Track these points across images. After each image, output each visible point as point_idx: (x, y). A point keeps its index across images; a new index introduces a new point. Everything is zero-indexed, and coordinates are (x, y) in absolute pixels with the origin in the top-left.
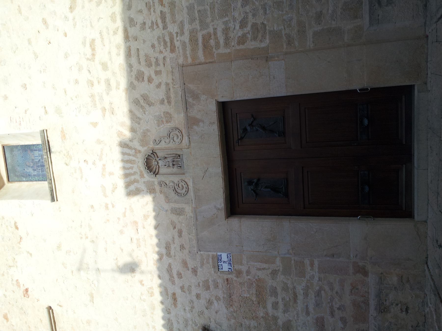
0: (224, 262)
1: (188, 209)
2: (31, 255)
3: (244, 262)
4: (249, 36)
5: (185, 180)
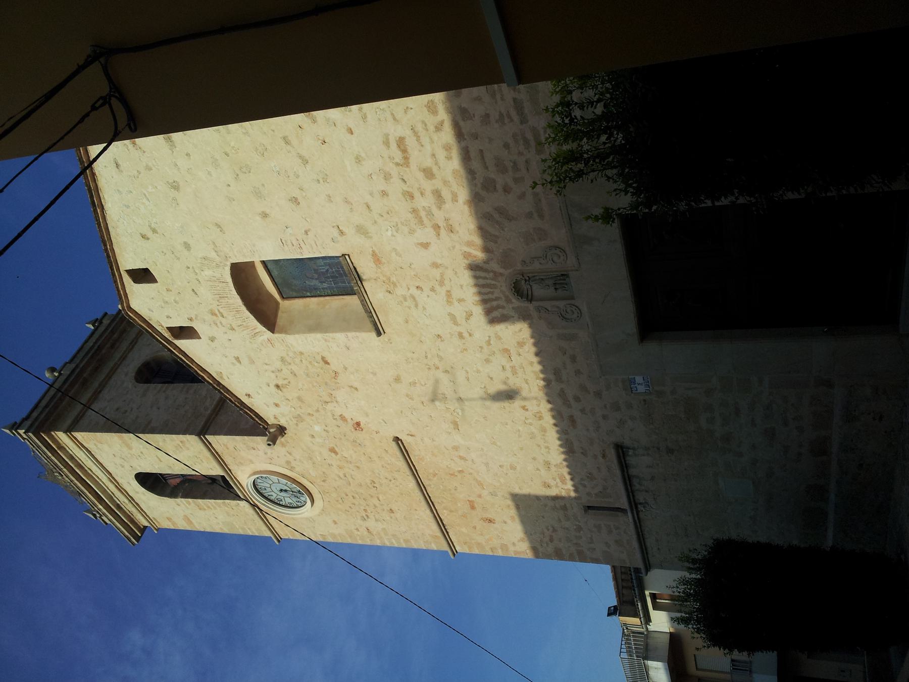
2: (356, 389)
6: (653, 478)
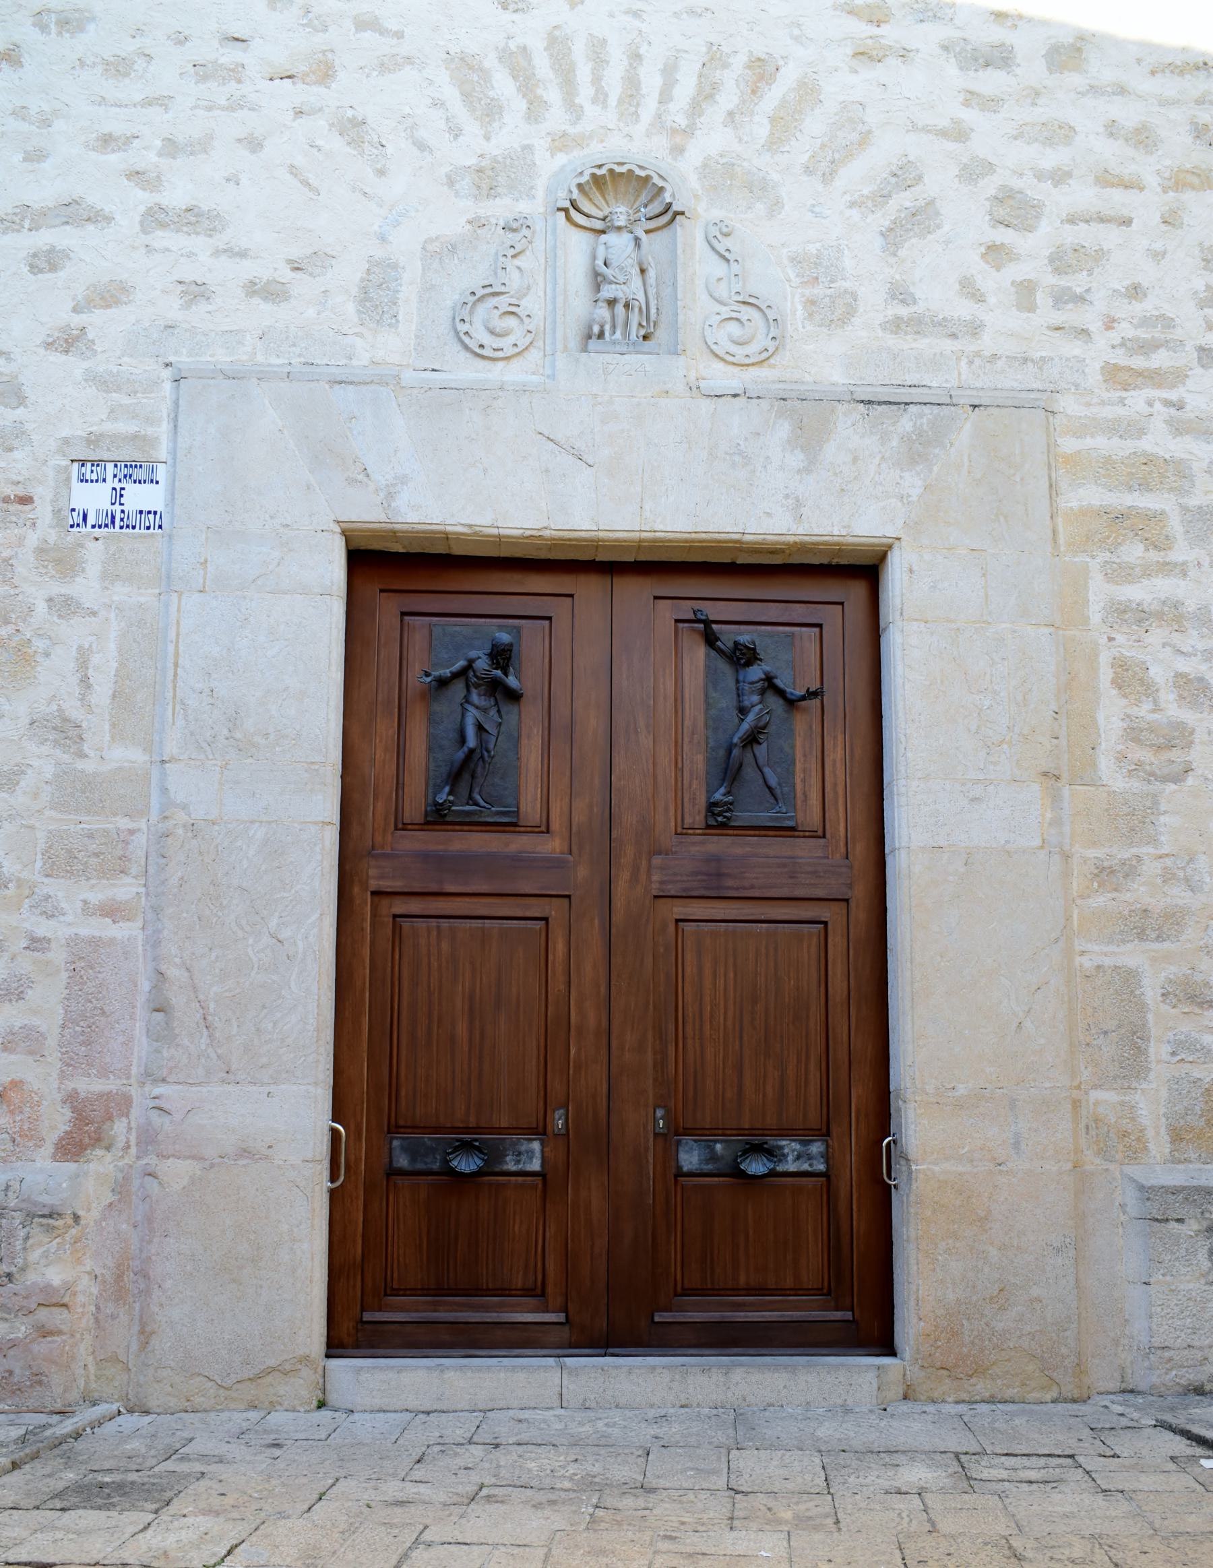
0: (119, 494)
1: (389, 347)
3: (120, 592)
4: (1144, 710)
5: (532, 350)
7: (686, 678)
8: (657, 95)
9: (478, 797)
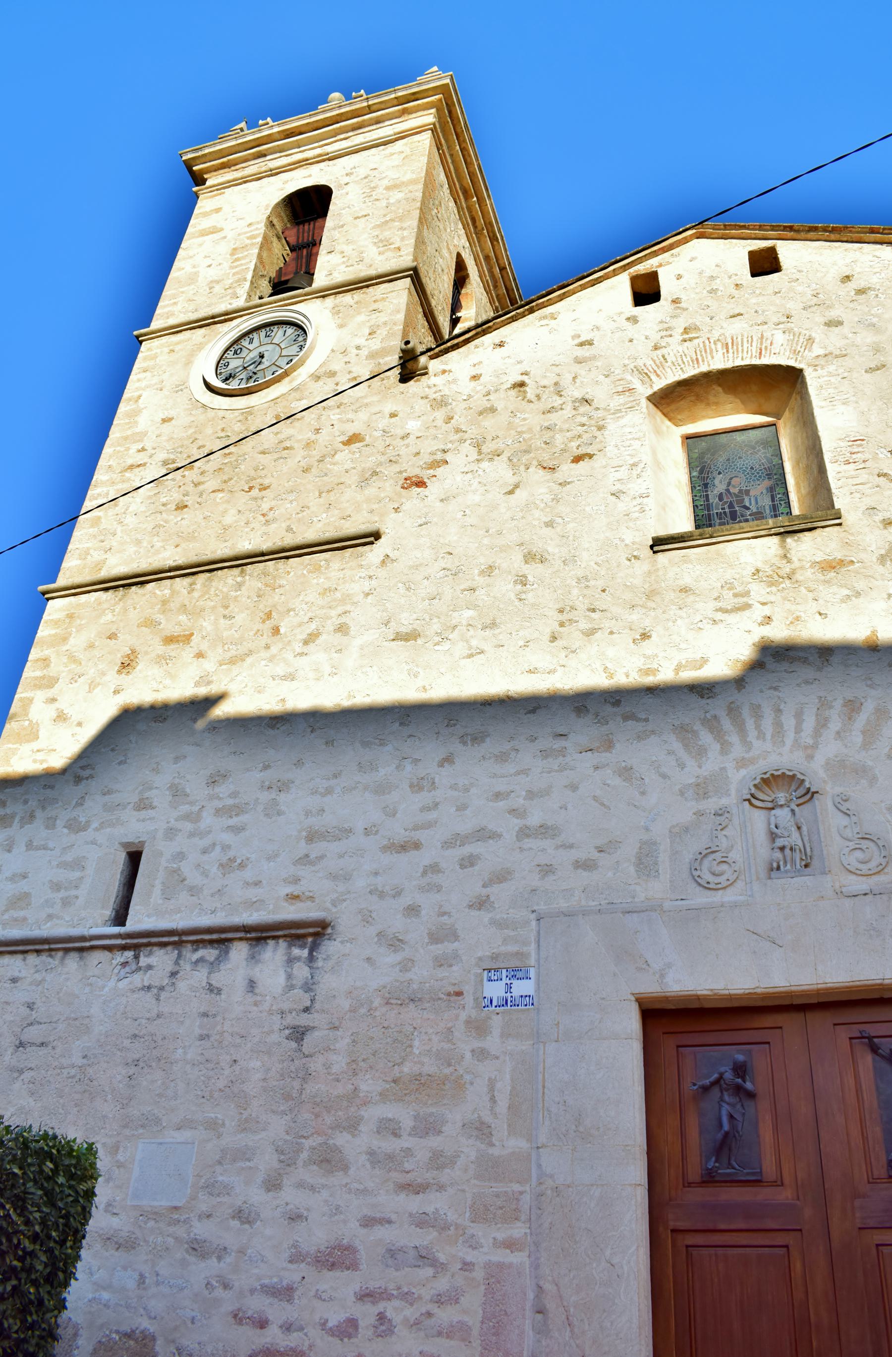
0: (509, 987)
1: (656, 889)
2: (511, 492)
5: (738, 881)
6: (212, 989)
7: (862, 1076)
8: (793, 730)
9: (734, 1164)
